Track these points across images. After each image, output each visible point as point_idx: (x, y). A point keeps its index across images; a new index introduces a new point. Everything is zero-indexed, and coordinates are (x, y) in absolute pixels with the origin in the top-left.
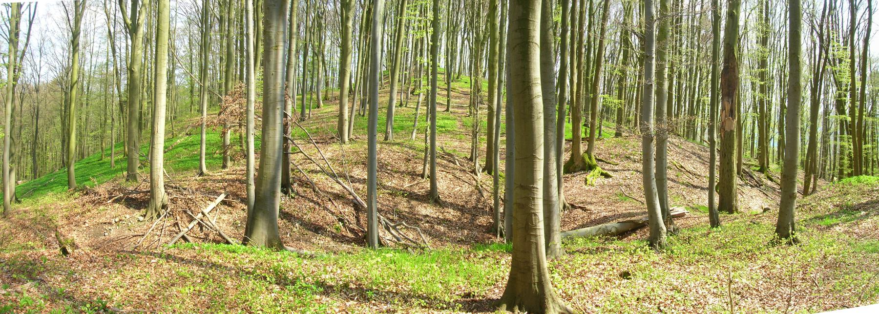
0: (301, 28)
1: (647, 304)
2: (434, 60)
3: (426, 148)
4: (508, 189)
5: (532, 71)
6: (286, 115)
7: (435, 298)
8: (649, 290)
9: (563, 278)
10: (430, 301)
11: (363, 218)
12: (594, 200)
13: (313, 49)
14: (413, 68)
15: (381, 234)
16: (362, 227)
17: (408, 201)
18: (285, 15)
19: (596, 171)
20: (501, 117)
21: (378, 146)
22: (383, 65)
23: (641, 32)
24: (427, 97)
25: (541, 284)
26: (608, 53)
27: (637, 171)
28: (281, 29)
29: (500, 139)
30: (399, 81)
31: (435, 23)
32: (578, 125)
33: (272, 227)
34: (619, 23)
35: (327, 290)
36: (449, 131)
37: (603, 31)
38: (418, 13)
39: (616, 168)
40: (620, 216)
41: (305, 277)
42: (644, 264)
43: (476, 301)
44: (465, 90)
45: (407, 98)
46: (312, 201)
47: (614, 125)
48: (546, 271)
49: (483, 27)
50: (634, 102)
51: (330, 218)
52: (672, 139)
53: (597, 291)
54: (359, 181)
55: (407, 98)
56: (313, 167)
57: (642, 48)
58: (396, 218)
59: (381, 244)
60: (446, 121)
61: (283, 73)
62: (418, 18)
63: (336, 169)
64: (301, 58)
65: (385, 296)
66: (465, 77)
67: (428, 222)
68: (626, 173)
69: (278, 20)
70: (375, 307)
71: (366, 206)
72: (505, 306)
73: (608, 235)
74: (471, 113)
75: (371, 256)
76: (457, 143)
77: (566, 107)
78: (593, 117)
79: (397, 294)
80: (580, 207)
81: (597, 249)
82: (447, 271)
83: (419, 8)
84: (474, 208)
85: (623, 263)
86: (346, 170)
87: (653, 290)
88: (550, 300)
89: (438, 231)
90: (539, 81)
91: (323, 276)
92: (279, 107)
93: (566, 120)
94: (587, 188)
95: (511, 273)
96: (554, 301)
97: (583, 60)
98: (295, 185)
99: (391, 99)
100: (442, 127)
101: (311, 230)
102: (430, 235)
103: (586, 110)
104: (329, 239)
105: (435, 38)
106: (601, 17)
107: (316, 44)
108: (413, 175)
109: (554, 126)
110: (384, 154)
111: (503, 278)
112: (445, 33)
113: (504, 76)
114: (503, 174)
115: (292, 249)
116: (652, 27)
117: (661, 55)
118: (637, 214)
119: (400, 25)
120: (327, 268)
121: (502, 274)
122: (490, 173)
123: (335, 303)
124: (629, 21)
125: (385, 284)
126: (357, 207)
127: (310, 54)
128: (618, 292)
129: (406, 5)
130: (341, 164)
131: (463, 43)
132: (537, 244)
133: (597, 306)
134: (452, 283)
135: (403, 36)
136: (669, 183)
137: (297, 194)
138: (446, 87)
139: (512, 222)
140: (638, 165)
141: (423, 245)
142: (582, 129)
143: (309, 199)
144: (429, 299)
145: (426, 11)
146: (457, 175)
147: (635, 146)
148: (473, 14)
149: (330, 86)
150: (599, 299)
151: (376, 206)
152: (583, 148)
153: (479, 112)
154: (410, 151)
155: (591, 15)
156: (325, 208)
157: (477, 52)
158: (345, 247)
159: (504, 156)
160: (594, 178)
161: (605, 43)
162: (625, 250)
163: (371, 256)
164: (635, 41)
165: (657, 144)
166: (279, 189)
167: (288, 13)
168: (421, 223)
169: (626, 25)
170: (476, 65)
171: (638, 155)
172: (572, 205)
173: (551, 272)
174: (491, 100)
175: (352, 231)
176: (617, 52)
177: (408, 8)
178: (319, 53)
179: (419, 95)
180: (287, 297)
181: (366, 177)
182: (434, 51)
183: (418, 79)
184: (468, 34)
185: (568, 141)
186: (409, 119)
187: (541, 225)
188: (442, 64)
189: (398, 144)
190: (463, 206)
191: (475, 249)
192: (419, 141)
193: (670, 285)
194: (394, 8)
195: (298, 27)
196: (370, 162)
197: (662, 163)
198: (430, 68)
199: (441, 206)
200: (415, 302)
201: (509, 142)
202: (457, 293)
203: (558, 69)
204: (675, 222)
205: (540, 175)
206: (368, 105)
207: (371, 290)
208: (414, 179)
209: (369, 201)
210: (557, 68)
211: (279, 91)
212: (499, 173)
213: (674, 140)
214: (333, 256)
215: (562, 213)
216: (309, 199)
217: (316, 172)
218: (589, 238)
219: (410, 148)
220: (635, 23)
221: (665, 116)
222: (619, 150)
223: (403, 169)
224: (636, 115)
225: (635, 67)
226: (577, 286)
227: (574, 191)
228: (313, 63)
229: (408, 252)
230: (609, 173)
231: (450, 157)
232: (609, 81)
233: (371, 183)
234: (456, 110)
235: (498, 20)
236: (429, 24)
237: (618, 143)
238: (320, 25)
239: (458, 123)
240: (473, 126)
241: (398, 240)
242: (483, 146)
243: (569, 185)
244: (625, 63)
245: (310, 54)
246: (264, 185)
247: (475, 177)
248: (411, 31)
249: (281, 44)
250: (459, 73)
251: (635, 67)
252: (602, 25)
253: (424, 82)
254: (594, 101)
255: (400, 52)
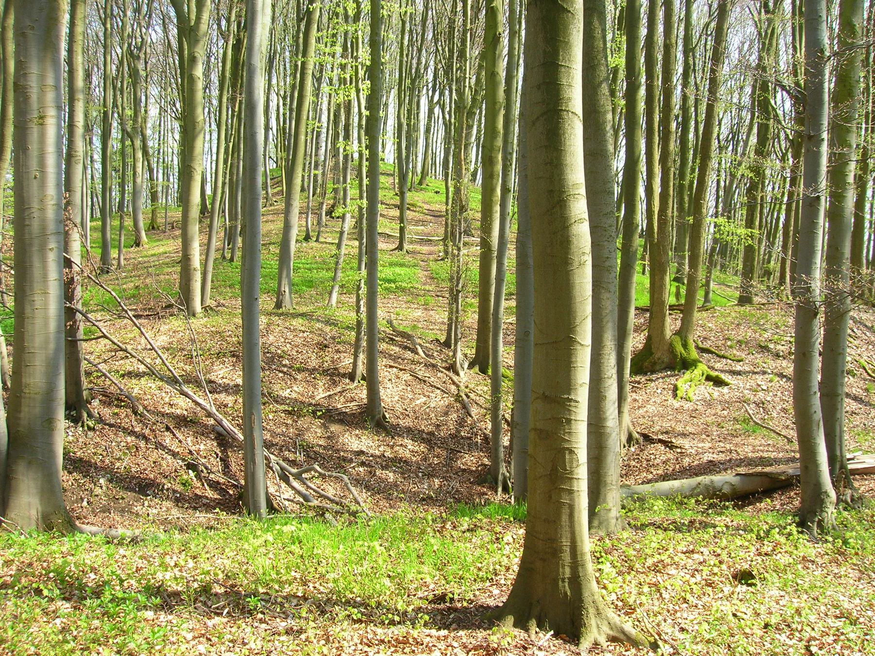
0: (95, 79)
1: (783, 638)
2: (372, 146)
3: (359, 323)
4: (520, 402)
5: (568, 171)
6: (68, 263)
7: (379, 604)
8: (790, 611)
9: (620, 573)
10: (369, 612)
11: (236, 460)
12: (690, 429)
13: (122, 124)
14: (330, 163)
15: (272, 490)
16: (233, 477)
17: (324, 426)
18: (56, 50)
19: (697, 372)
20: (506, 262)
21: (263, 320)
22: (269, 161)
23: (797, 84)
24: (359, 222)
25: (576, 582)
26: (725, 131)
27: (781, 376)
28: (50, 81)
29: (504, 304)
30: (303, 190)
31: (374, 71)
32: (662, 279)
33: (50, 490)
34: (748, 67)
35: (167, 600)
36: (403, 290)
37: (714, 84)
38: (338, 49)
39: (738, 368)
40: (740, 462)
41: (122, 581)
42: (783, 559)
43: (456, 610)
44: (436, 207)
45: (319, 223)
46: (132, 433)
47: (737, 280)
48: (588, 557)
49: (471, 80)
50: (780, 234)
51: (169, 463)
52: (857, 313)
53: (685, 601)
54: (226, 389)
55: (319, 223)
56: (129, 365)
57: (799, 119)
58: (300, 457)
59: (271, 509)
60: (398, 270)
61: (59, 174)
62: (339, 60)
63: (178, 368)
64: (97, 143)
65: (282, 605)
66: (435, 182)
67: (363, 464)
68: (759, 378)
69: (41, 60)
70: (264, 626)
71: (241, 437)
72: (510, 620)
73: (717, 498)
74: (446, 252)
75: (253, 531)
76: (419, 313)
77: (638, 242)
78: (693, 264)
79: (305, 599)
80: (660, 441)
81: (692, 522)
82: (400, 555)
83: (340, 40)
84: (453, 436)
85: (742, 554)
86: (198, 369)
87: (798, 612)
88: (592, 611)
89: (382, 480)
90: (583, 191)
91: (159, 576)
92: (52, 244)
93: (638, 268)
94: (676, 404)
95: (524, 560)
96: (599, 613)
97: (673, 146)
98: (96, 403)
99: (287, 227)
100: (389, 281)
101: (132, 490)
102: (368, 488)
103: (679, 248)
104: (168, 504)
105: (374, 102)
106: (709, 54)
107: (129, 112)
108: (333, 375)
109: (612, 284)
110: (275, 335)
111: (508, 569)
112: (394, 93)
113: (514, 180)
114: (510, 374)
115: (94, 529)
116: (821, 73)
117: (839, 134)
118: (777, 461)
119: (303, 74)
120: (167, 559)
121: (505, 561)
122: (483, 371)
123: (185, 624)
124: (769, 61)
125: (280, 583)
126: (223, 440)
127: (115, 134)
128: (728, 608)
129: (314, 33)
130: (189, 358)
131: (431, 111)
132: (572, 508)
133: (682, 630)
134: (410, 576)
135: (309, 98)
136: (849, 405)
137: (101, 420)
138: (397, 200)
139: (524, 465)
140: (784, 363)
141: (353, 508)
142: (670, 288)
143: (125, 430)
144: (366, 606)
145: (355, 46)
146: (420, 374)
147: (778, 324)
148: (451, 51)
149: (162, 200)
150: (688, 617)
151: (258, 438)
152: (671, 324)
153: (464, 251)
154: (328, 329)
155: (688, 50)
156: (159, 446)
157: (459, 131)
158: (202, 517)
159: (512, 338)
160: (692, 385)
161: (719, 109)
162: (747, 529)
163: (253, 531)
164: (783, 103)
165: (828, 323)
166: (61, 413)
167: (63, 45)
168: (349, 467)
169: (764, 69)
170: (457, 156)
171: (786, 342)
172: (646, 437)
173: (598, 560)
174: (486, 228)
175: (214, 485)
176: (745, 129)
177: (318, 40)
178: (134, 132)
179: (343, 218)
180: (86, 622)
181: (240, 381)
182: (372, 128)
183: (340, 186)
184: (442, 94)
185: (641, 310)
186: (323, 265)
187: (582, 473)
188: (388, 155)
189: (302, 315)
190: (431, 434)
191: (454, 513)
192: (343, 310)
193: (836, 607)
194: (289, 40)
195: (88, 76)
196: (246, 352)
197: (835, 363)
198: (365, 163)
199: (388, 433)
200: (341, 612)
201: (522, 312)
202: (420, 594)
203: (621, 165)
204: (856, 484)
205: (583, 375)
206: (240, 240)
207: (255, 594)
208: (335, 384)
209: (248, 426)
210: (618, 163)
211: (51, 213)
212: (502, 370)
213: (864, 316)
214: (177, 536)
215: (624, 451)
216: (125, 430)
217: (138, 375)
218: (677, 500)
219: (328, 322)
220: (783, 66)
221: (846, 266)
222: (746, 333)
223: (313, 363)
224: (784, 261)
225: (783, 159)
226: (646, 589)
227: (651, 408)
228: (123, 153)
229: (325, 522)
230: (723, 376)
231: (405, 339)
232: (728, 191)
233: (250, 393)
234: (418, 248)
235: (502, 65)
236: (361, 73)
237: (743, 317)
238: (134, 74)
239: (421, 274)
240: (451, 279)
241: (306, 498)
242: (471, 318)
243: (640, 396)
244: (761, 151)
245: (115, 134)
246: (25, 409)
247: (455, 378)
248: (325, 88)
249: (51, 112)
250: (424, 174)
251: (783, 159)
252: (713, 71)
253: (353, 192)
254: (696, 230)
255: (303, 129)
